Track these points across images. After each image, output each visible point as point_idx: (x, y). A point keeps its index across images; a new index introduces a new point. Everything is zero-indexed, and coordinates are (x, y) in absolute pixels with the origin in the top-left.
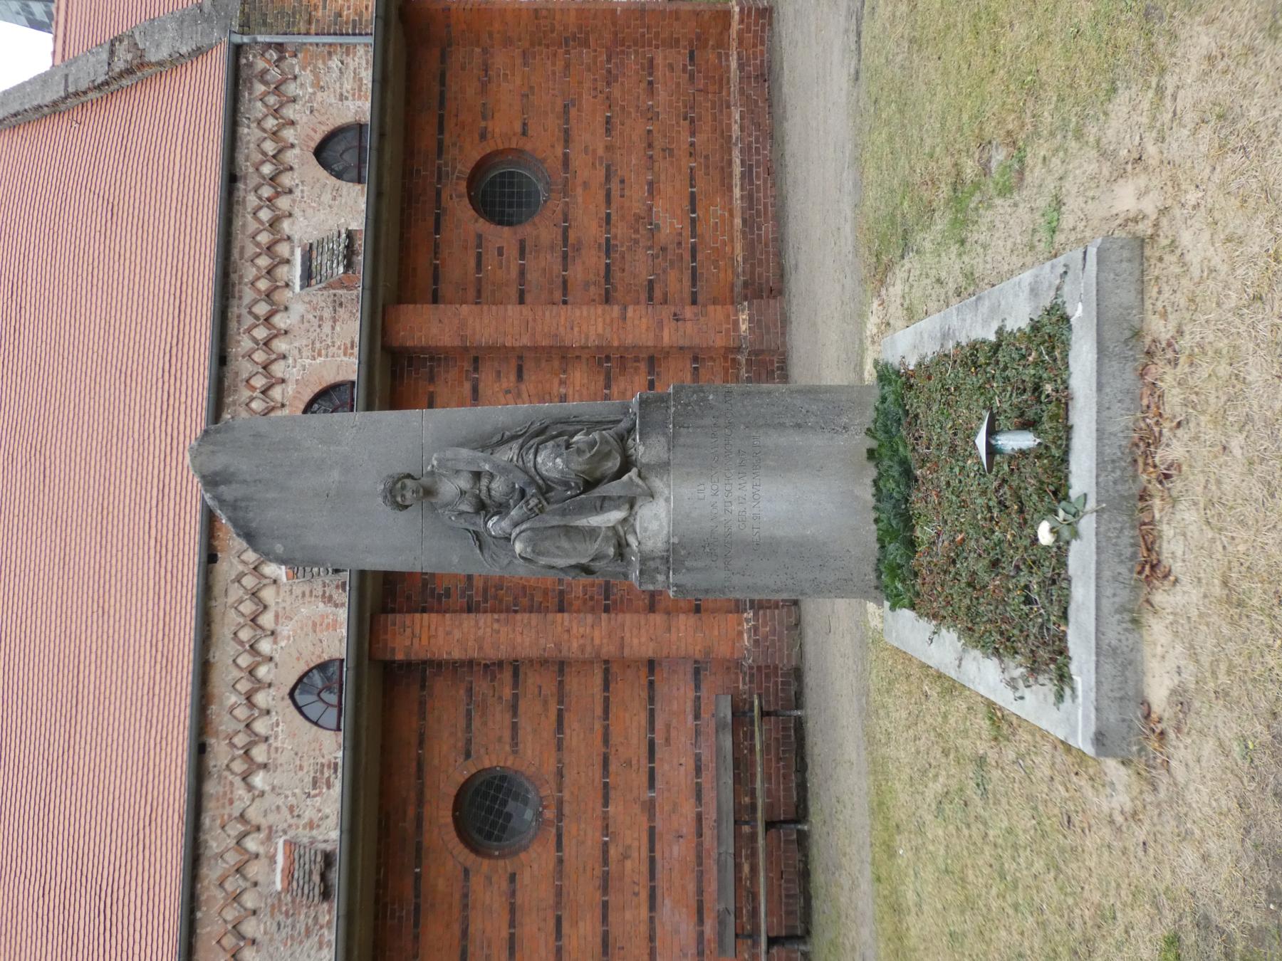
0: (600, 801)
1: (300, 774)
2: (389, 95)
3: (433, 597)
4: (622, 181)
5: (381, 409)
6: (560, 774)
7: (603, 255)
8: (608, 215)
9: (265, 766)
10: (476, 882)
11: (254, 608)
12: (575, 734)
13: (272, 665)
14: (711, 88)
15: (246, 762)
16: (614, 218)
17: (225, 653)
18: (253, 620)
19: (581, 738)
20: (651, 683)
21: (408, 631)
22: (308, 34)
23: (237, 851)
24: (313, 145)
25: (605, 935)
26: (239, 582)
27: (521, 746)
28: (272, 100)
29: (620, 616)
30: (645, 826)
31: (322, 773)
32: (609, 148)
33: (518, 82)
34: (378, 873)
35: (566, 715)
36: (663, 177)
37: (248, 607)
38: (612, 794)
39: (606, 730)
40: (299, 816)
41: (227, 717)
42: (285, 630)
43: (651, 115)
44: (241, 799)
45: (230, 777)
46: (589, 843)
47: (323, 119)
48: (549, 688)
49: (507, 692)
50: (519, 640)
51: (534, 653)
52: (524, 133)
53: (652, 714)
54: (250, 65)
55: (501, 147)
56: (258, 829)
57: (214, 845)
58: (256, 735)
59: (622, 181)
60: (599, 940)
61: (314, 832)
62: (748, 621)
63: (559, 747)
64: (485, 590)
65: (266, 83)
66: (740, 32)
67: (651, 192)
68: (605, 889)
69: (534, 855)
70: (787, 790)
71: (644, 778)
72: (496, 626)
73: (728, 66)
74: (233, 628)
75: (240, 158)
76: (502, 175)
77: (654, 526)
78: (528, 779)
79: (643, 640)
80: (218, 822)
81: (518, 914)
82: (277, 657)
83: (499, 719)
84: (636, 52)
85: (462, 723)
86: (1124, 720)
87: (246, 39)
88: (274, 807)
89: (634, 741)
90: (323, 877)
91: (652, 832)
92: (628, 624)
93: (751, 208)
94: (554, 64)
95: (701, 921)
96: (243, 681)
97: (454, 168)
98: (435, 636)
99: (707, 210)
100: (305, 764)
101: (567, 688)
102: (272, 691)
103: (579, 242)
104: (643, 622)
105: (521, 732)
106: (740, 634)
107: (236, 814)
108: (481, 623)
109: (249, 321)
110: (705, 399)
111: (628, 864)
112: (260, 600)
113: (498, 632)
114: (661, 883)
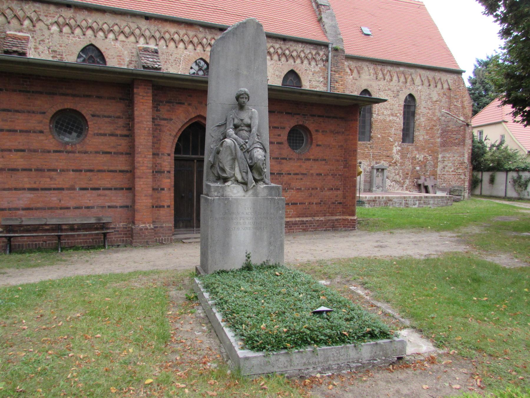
0: (75, 168)
1: (58, 46)
2: (316, 98)
3: (157, 105)
4: (301, 179)
5: (269, 94)
6: (86, 152)
7: (277, 172)
8: (291, 174)
9: (61, 31)
10: (39, 117)
11: (127, 33)
12: (102, 158)
13: (104, 38)
14: (330, 210)
15: (63, 23)
16: (290, 176)
17: (109, 20)
18: (122, 32)
19: (101, 161)
20: (122, 189)
21: (145, 94)
22: (331, 71)
23: (24, 16)
24: (295, 70)
25: (18, 170)
26: (138, 28)
27: (97, 137)
28: (310, 56)
29: (151, 177)
30: (64, 187)
31: (59, 55)
32: (312, 174)
33: (334, 144)
34: (43, 76)
35: (109, 155)
36: (303, 193)
37: (127, 30)
38: (78, 173)
39: (104, 171)
40: (40, 43)
41: (82, 17)
42: (118, 44)
43: (322, 189)
44: (48, 20)
45: (57, 17)
46: (56, 164)
47: (304, 74)
48: (120, 149)
49: (119, 132)
50: (142, 138)
51: (137, 143)
52: (317, 145)
53: (110, 189)
54: (321, 50)
55: (313, 137)
56: (34, 26)
57: (27, 7)
58: (75, 29)
59: (301, 179)
60: (15, 167)
61: (33, 50)
62: (150, 226)
63: (97, 152)
64: (159, 125)
65: (315, 55)
66: (347, 220)
67: (298, 189)
68: (37, 170)
69: (51, 141)
70: (81, 243)
71: (84, 186)
72: (147, 129)
73: (336, 216)
74: (119, 24)
75: (291, 43)
76: (303, 137)
77: (235, 191)
78: (83, 139)
79: (142, 186)
80: (37, 10)
81: (25, 134)
82: (107, 40)
83: (108, 129)
84: (341, 184)
85: (106, 114)
86: (253, 366)
87: (330, 49)
88: (43, 33)
89: (99, 182)
90: (15, 52)
91: (62, 189)
92: (149, 180)
93: (292, 224)
94: (339, 156)
95: (24, 209)
96: (97, 26)
97: (307, 120)
98: (143, 105)
99: (292, 209)
100: (62, 48)
101: (121, 156)
102: (93, 37)
103: (282, 164)
104: (149, 186)
105: (103, 137)
106: (144, 223)
107: (41, 18)
108: (149, 123)
109: (163, 30)
110: (280, 209)
111: (48, 180)
112: (130, 35)
113: (145, 130)
114: (40, 193)
